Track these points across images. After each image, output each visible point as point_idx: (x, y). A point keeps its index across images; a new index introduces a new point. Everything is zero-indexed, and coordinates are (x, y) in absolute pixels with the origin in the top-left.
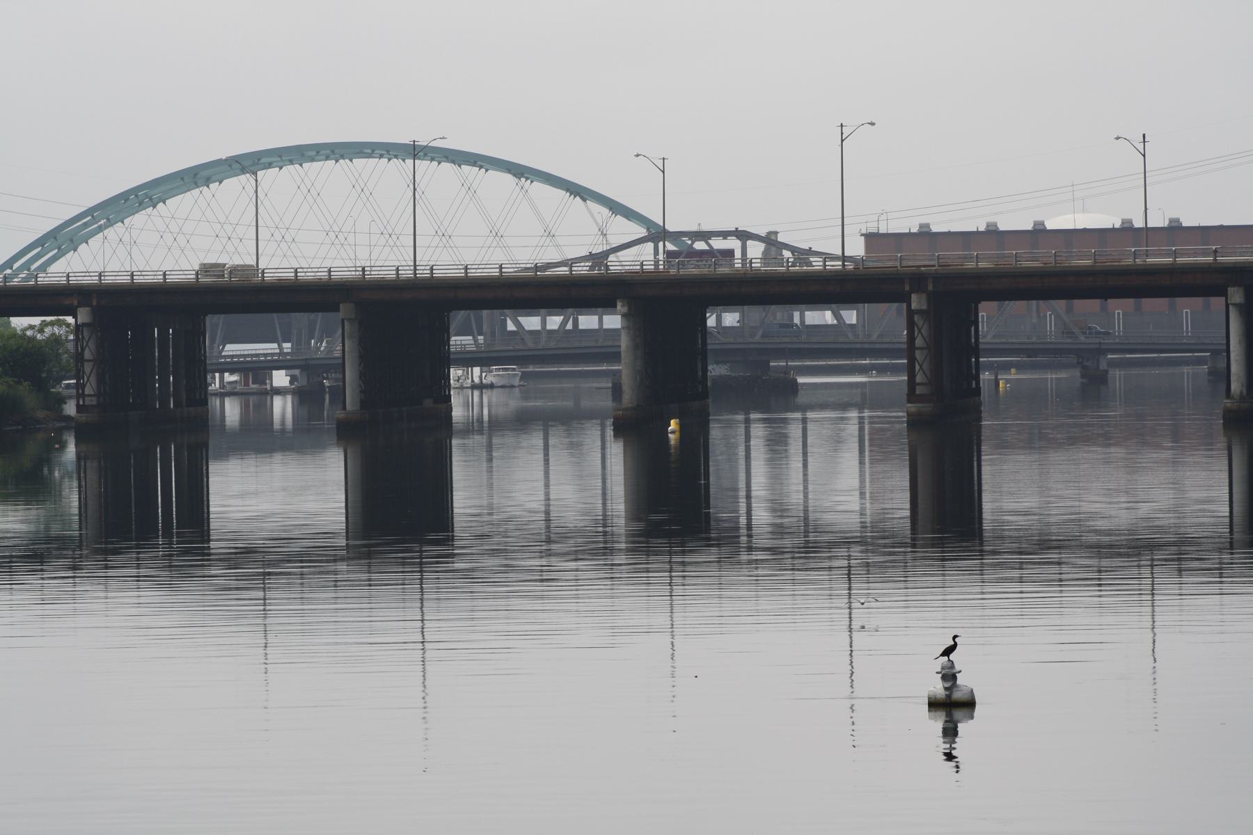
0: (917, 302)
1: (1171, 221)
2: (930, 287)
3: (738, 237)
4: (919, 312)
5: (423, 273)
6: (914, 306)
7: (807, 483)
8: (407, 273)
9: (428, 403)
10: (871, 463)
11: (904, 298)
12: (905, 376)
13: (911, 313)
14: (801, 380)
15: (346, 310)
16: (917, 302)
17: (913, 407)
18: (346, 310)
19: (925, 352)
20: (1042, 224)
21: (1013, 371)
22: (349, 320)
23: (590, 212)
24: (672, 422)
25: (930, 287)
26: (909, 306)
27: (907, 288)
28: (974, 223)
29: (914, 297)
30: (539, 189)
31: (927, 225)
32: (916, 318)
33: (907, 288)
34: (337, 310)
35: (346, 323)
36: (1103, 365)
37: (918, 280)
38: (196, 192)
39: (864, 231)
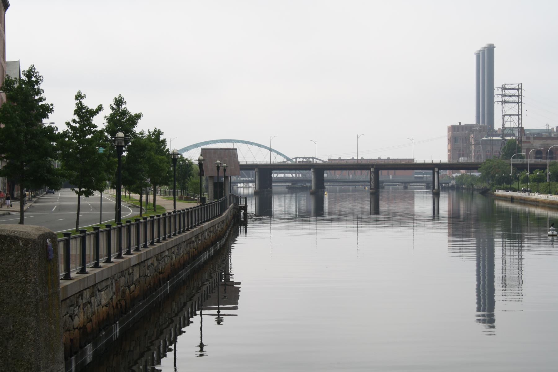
0: (372, 170)
1: (388, 157)
2: (375, 167)
3: (312, 158)
4: (372, 172)
5: (272, 163)
6: (372, 171)
7: (259, 220)
8: (269, 163)
9: (269, 189)
10: (311, 211)
11: (369, 169)
12: (138, 212)
13: (371, 172)
14: (326, 187)
15: (256, 170)
16: (372, 170)
17: (371, 191)
18: (256, 170)
19: (374, 180)
20: (340, 157)
21: (361, 186)
22: (257, 172)
23: (281, 154)
24: (326, 192)
25: (375, 167)
26: (371, 171)
27: (370, 167)
28: (337, 158)
29: (372, 169)
30: (262, 149)
31: (340, 157)
32: (372, 173)
33: (370, 167)
34: (254, 170)
35: (256, 173)
36: (384, 185)
37: (373, 165)
38: (196, 148)
39: (328, 158)
